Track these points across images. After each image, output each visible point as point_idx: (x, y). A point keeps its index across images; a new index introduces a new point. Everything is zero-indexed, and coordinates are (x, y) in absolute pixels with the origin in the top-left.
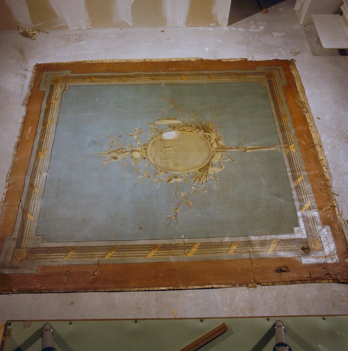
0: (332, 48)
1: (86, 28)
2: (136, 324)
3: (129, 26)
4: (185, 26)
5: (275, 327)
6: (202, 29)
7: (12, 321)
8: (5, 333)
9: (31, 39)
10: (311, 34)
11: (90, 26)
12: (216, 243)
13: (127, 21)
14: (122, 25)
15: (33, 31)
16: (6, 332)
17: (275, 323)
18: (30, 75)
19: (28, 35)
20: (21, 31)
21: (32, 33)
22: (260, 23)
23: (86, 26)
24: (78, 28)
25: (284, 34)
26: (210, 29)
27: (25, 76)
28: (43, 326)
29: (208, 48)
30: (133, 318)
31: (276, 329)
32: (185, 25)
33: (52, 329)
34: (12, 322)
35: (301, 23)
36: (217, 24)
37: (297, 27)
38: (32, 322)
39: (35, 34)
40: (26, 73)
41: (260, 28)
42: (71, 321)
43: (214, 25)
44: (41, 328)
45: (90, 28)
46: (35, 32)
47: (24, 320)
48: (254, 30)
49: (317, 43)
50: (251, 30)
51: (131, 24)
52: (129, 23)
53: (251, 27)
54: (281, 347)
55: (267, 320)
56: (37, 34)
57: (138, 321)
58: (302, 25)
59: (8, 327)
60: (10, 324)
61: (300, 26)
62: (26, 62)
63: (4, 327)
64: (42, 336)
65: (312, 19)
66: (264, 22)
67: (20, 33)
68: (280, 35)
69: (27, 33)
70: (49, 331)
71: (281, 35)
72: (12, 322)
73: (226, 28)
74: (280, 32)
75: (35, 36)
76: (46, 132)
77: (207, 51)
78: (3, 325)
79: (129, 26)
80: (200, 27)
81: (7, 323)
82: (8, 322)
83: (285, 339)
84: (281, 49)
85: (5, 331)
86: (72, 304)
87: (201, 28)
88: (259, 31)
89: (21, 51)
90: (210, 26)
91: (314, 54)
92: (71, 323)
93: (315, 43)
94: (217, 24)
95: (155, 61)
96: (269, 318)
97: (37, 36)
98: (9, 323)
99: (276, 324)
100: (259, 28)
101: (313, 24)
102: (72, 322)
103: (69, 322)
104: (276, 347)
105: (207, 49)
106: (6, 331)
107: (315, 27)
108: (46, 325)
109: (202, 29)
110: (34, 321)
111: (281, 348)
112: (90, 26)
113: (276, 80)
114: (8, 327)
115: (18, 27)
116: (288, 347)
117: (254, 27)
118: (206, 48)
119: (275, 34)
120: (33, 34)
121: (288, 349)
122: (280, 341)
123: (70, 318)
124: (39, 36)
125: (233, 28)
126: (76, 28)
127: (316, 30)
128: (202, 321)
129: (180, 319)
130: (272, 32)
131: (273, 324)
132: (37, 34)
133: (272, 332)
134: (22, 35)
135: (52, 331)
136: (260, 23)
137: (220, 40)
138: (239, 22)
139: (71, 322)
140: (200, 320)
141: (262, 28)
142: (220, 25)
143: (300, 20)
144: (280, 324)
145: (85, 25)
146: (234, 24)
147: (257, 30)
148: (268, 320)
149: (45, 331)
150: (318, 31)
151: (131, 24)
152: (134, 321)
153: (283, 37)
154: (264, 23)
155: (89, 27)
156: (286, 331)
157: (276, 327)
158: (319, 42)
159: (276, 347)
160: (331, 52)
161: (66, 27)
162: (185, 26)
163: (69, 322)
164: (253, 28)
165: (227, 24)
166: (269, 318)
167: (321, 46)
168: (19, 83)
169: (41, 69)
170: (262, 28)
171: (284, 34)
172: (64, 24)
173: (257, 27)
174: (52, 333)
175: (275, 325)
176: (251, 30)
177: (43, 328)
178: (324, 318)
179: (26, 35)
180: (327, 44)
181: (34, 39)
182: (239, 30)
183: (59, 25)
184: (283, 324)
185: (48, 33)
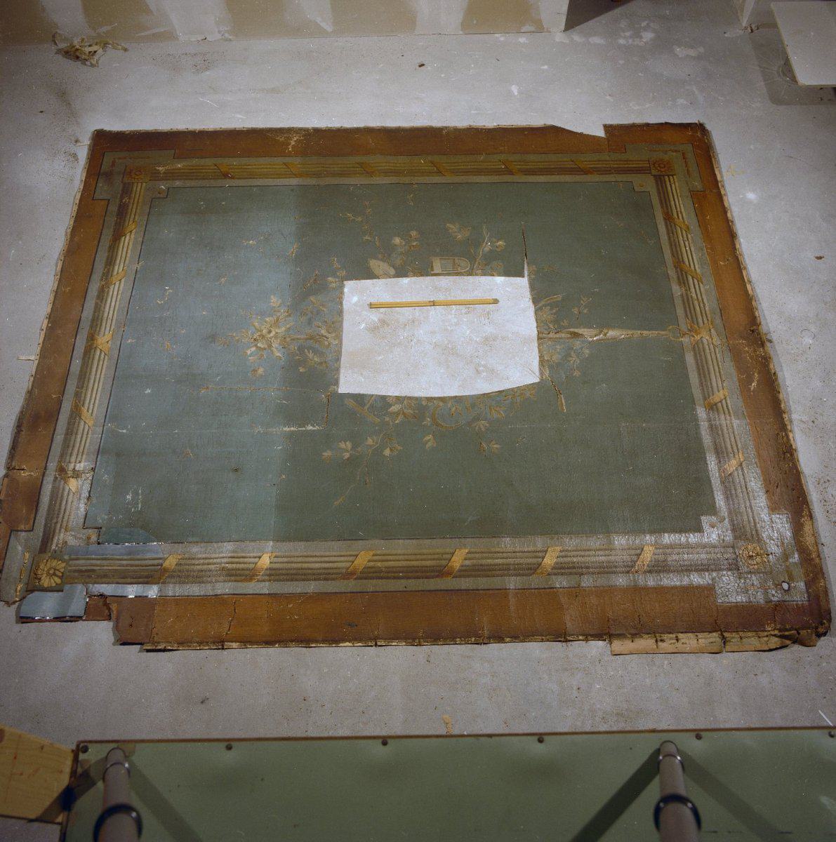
1: (219, 36)
4: (461, 33)
5: (659, 755)
6: (502, 39)
7: (90, 742)
9: (86, 65)
12: (115, 581)
13: (319, 20)
14: (302, 29)
15: (90, 46)
16: (77, 768)
17: (658, 747)
19: (78, 54)
21: (87, 50)
22: (644, 24)
24: (199, 39)
26: (522, 40)
27: (75, 156)
28: (106, 754)
30: (692, 727)
31: (661, 760)
32: (462, 30)
33: (126, 761)
34: (90, 745)
35: (744, 24)
36: (540, 28)
37: (734, 33)
38: (138, 745)
39: (95, 52)
40: (73, 149)
41: (643, 36)
42: (232, 743)
43: (532, 29)
44: (102, 759)
45: (230, 37)
46: (94, 48)
47: (119, 739)
48: (630, 41)
50: (622, 41)
52: (323, 25)
53: (622, 34)
55: (695, 738)
56: (100, 51)
57: (389, 741)
58: (746, 28)
59: (82, 756)
61: (740, 31)
63: (72, 755)
64: (104, 779)
65: (770, 13)
66: (654, 22)
67: (59, 52)
69: (77, 50)
71: (692, 53)
72: (90, 745)
73: (559, 37)
75: (96, 57)
76: (111, 293)
77: (516, 94)
80: (497, 35)
81: (78, 746)
82: (82, 745)
83: (681, 785)
85: (75, 766)
86: (202, 702)
88: (641, 44)
89: (63, 95)
91: (776, 99)
92: (229, 748)
93: (778, 72)
94: (540, 28)
96: (702, 733)
98: (83, 747)
99: (661, 750)
100: (641, 37)
101: (775, 26)
104: (662, 805)
106: (77, 764)
107: (779, 35)
109: (502, 39)
110: (143, 741)
111: (673, 807)
113: (662, 170)
114: (82, 756)
115: (54, 36)
117: (628, 34)
118: (514, 86)
120: (90, 52)
122: (669, 791)
123: (384, 733)
124: (106, 58)
125: (576, 36)
127: (781, 42)
128: (541, 741)
129: (490, 736)
130: (674, 47)
133: (652, 767)
134: (63, 56)
135: (127, 765)
136: (644, 24)
137: (546, 67)
138: (591, 23)
139: (229, 744)
140: (224, 745)
141: (648, 36)
142: (545, 30)
143: (740, 17)
144: (671, 748)
145: (217, 30)
146: (582, 26)
147: (637, 42)
149: (111, 765)
151: (330, 30)
153: (699, 58)
154: (652, 24)
155: (227, 35)
157: (661, 758)
158: (787, 69)
159: (662, 805)
161: (170, 36)
164: (625, 37)
165: (563, 26)
166: (702, 733)
167: (794, 79)
168: (55, 178)
169: (104, 142)
170: (648, 36)
171: (701, 50)
174: (129, 771)
175: (658, 752)
176: (622, 41)
177: (106, 757)
179: (73, 54)
181: (92, 65)
182: (592, 42)
184: (677, 749)
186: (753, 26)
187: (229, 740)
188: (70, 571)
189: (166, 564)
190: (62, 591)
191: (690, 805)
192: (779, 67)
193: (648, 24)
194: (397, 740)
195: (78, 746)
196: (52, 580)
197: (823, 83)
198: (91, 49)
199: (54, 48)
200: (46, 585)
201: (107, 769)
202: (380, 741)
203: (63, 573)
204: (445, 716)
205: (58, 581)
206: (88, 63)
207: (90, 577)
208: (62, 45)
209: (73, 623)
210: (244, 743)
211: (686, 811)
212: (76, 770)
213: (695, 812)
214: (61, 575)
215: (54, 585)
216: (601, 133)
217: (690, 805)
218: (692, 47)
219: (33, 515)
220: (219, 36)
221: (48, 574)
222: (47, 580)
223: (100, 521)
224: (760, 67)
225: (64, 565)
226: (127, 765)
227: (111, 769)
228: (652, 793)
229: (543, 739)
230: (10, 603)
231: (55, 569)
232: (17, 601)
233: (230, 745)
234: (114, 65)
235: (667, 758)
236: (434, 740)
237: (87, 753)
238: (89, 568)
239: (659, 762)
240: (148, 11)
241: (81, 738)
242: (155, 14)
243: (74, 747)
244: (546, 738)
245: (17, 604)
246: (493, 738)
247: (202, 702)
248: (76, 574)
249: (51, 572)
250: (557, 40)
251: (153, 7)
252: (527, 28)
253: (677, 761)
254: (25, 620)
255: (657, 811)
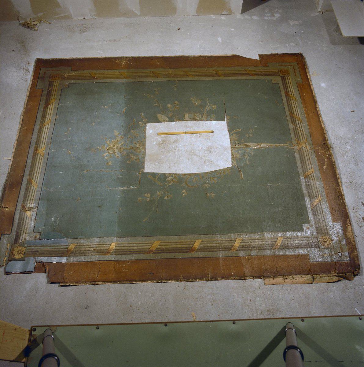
0: (352, 37)
1: (91, 17)
2: (165, 327)
3: (136, 15)
6: (214, 17)
8: (31, 339)
9: (32, 30)
10: (330, 22)
11: (94, 15)
13: (134, 10)
14: (128, 13)
15: (34, 22)
17: (285, 325)
18: (31, 69)
19: (28, 25)
20: (22, 21)
21: (33, 23)
23: (91, 15)
25: (301, 21)
26: (223, 18)
27: (28, 70)
28: (44, 332)
29: (221, 38)
30: (300, 316)
32: (196, 14)
36: (230, 12)
37: (315, 14)
38: (58, 327)
39: (36, 24)
41: (276, 16)
42: (304, 319)
43: (227, 13)
44: (42, 334)
45: (95, 18)
49: (336, 31)
50: (266, 18)
51: (138, 13)
52: (136, 12)
54: (292, 350)
56: (39, 24)
57: (168, 324)
58: (320, 12)
59: (33, 333)
60: (35, 330)
62: (28, 55)
67: (20, 24)
68: (297, 23)
69: (28, 23)
70: (49, 337)
71: (297, 23)
73: (239, 16)
74: (296, 20)
75: (37, 27)
77: (220, 41)
78: (28, 331)
79: (136, 15)
80: (211, 16)
81: (31, 328)
83: (295, 341)
84: (298, 38)
87: (213, 17)
88: (275, 19)
89: (23, 44)
90: (223, 14)
91: (333, 43)
92: (98, 328)
94: (230, 12)
95: (28, 93)
97: (38, 27)
98: (33, 329)
99: (286, 326)
100: (274, 16)
101: (332, 11)
102: (305, 319)
103: (96, 326)
105: (220, 39)
108: (46, 331)
109: (214, 17)
111: (291, 351)
112: (94, 15)
113: (285, 74)
114: (33, 333)
115: (18, 18)
116: (299, 350)
117: (269, 15)
119: (292, 23)
120: (34, 25)
121: (288, 350)
124: (42, 27)
125: (246, 16)
126: (80, 18)
128: (234, 323)
129: (212, 321)
131: (283, 326)
132: (39, 24)
133: (282, 334)
135: (53, 336)
136: (276, 11)
138: (252, 10)
141: (277, 16)
144: (291, 326)
145: (89, 14)
147: (273, 18)
148: (303, 321)
150: (337, 18)
152: (232, 322)
154: (279, 11)
155: (94, 17)
156: (297, 334)
157: (286, 330)
158: (338, 29)
160: (351, 41)
161: (69, 17)
162: (196, 15)
163: (96, 326)
164: (268, 16)
167: (341, 34)
168: (20, 80)
169: (41, 64)
171: (301, 21)
172: (66, 14)
173: (273, 15)
175: (285, 327)
178: (361, 318)
179: (26, 25)
180: (348, 31)
181: (35, 30)
183: (62, 15)
185: (50, 23)
188: (28, 252)
190: (24, 260)
196: (20, 256)
200: (17, 258)
203: (24, 252)
205: (23, 256)
207: (36, 254)
209: (29, 274)
214: (23, 253)
215: (20, 258)
216: (257, 58)
219: (11, 227)
221: (18, 253)
222: (18, 256)
223: (41, 229)
225: (25, 249)
230: (1, 266)
231: (21, 251)
232: (4, 265)
238: (36, 250)
245: (4, 266)
248: (30, 253)
249: (19, 252)
254: (7, 273)
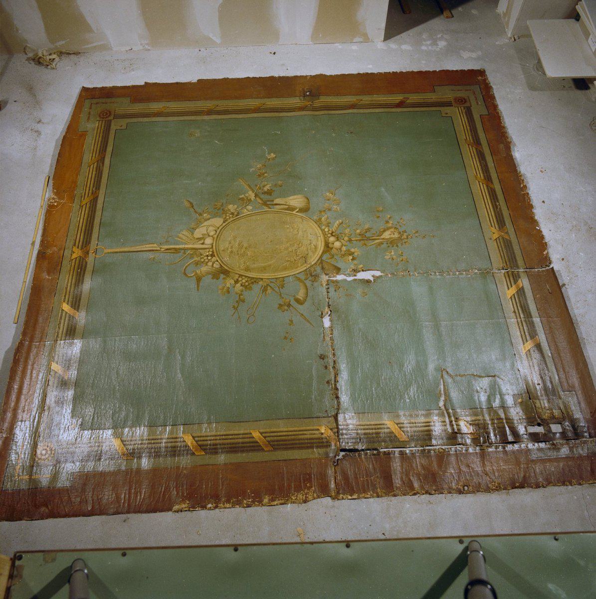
1: (141, 48)
5: (467, 552)
6: (340, 47)
7: (24, 552)
13: (211, 36)
16: (14, 572)
21: (48, 57)
26: (354, 47)
35: (509, 35)
36: (366, 39)
38: (59, 554)
39: (54, 59)
43: (361, 40)
45: (149, 48)
46: (54, 56)
48: (430, 47)
50: (424, 48)
53: (424, 42)
56: (57, 59)
58: (511, 38)
59: (17, 563)
64: (69, 581)
65: (527, 28)
67: (28, 59)
71: (474, 55)
73: (380, 45)
80: (336, 45)
82: (18, 555)
83: (484, 572)
86: (125, 521)
89: (31, 89)
91: (532, 88)
92: (124, 555)
94: (366, 39)
98: (18, 556)
100: (437, 45)
101: (530, 36)
104: (469, 587)
109: (340, 47)
110: (62, 551)
111: (479, 588)
114: (17, 563)
115: (25, 49)
117: (429, 42)
120: (50, 59)
125: (392, 44)
129: (312, 543)
133: (462, 562)
135: (86, 571)
136: (439, 36)
138: (404, 35)
141: (442, 44)
147: (434, 48)
151: (218, 41)
154: (445, 36)
157: (469, 553)
158: (539, 66)
159: (469, 587)
161: (105, 47)
164: (426, 45)
165: (382, 38)
167: (544, 73)
170: (442, 44)
171: (480, 53)
174: (87, 575)
179: (38, 61)
186: (516, 37)
187: (124, 549)
189: (433, 440)
191: (489, 587)
192: (534, 65)
193: (442, 35)
194: (244, 547)
195: (15, 555)
197: (564, 76)
198: (51, 57)
199: (26, 57)
201: (72, 575)
202: (233, 548)
204: (298, 529)
206: (49, 67)
208: (31, 55)
210: (135, 551)
211: (487, 591)
212: (13, 573)
213: (493, 591)
217: (489, 587)
218: (473, 51)
220: (141, 48)
224: (521, 64)
226: (86, 571)
227: (74, 574)
228: (462, 580)
229: (349, 544)
233: (125, 552)
234: (67, 68)
235: (473, 553)
236: (271, 546)
237: (21, 561)
239: (467, 556)
240: (88, 29)
241: (19, 549)
242: (96, 32)
243: (12, 556)
244: (352, 544)
246: (314, 545)
247: (125, 521)
250: (379, 48)
251: (93, 26)
252: (357, 39)
253: (480, 555)
255: (466, 591)
